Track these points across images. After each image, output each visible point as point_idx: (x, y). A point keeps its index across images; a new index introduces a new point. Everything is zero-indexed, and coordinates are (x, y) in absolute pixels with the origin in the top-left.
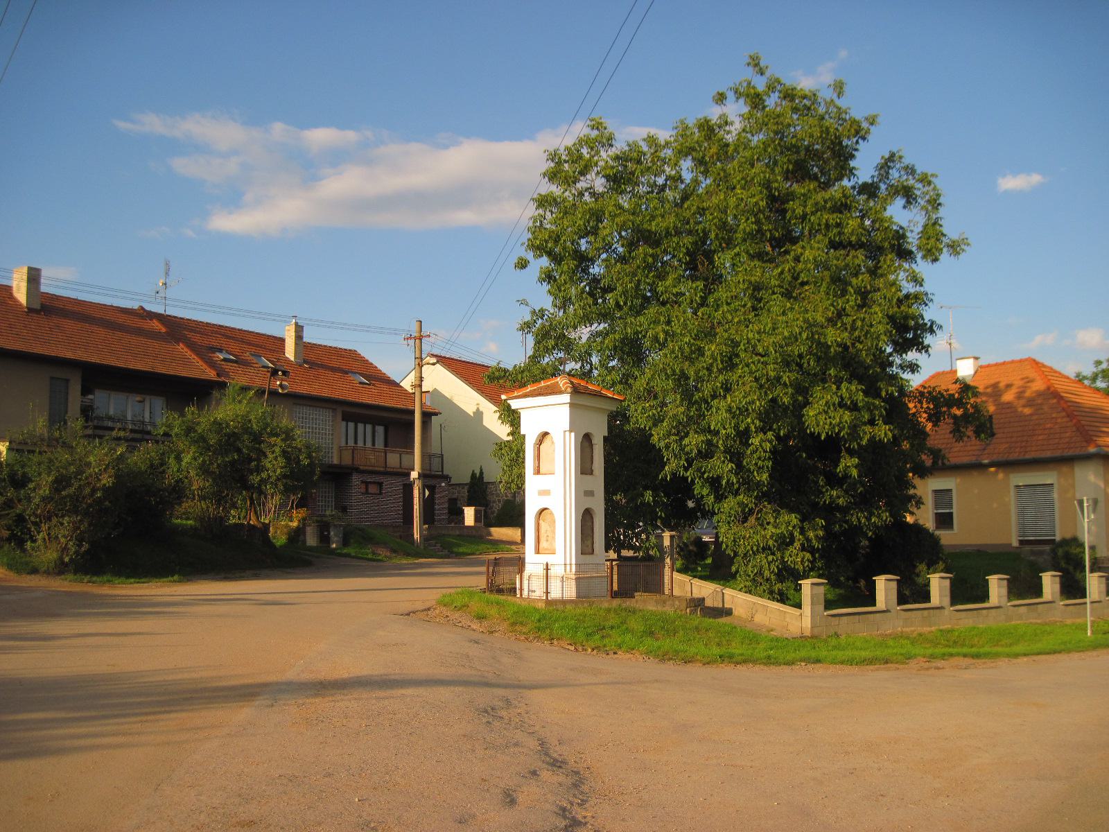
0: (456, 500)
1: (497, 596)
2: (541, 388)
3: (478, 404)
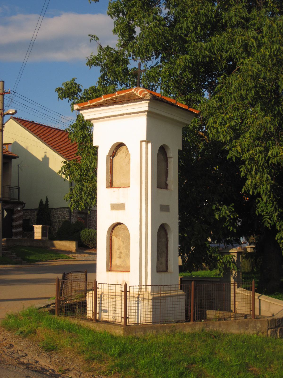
0: (28, 220)
1: (68, 319)
2: (116, 98)
3: (45, 152)
